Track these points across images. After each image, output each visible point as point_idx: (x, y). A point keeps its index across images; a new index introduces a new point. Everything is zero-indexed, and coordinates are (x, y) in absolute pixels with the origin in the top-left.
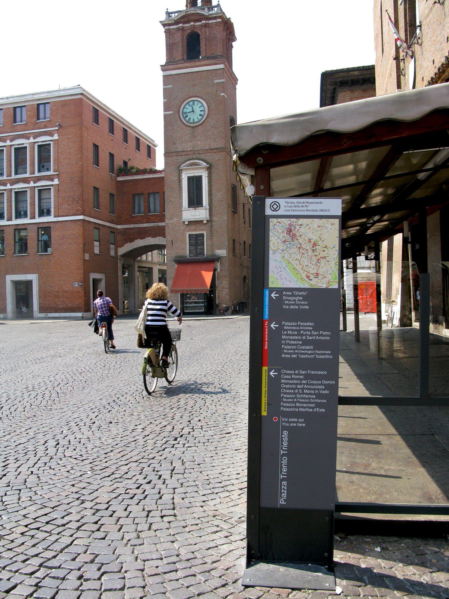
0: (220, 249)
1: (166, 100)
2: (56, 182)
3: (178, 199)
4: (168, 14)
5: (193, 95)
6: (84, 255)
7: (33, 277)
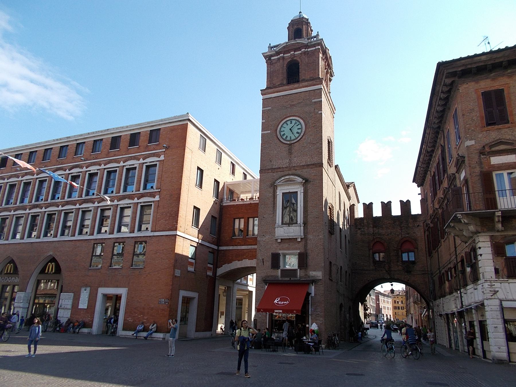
0: (315, 271)
1: (264, 121)
2: (157, 198)
3: (271, 216)
4: (271, 48)
5: (291, 115)
6: (174, 271)
7: (123, 291)
